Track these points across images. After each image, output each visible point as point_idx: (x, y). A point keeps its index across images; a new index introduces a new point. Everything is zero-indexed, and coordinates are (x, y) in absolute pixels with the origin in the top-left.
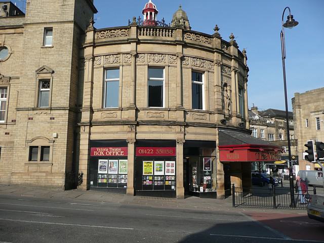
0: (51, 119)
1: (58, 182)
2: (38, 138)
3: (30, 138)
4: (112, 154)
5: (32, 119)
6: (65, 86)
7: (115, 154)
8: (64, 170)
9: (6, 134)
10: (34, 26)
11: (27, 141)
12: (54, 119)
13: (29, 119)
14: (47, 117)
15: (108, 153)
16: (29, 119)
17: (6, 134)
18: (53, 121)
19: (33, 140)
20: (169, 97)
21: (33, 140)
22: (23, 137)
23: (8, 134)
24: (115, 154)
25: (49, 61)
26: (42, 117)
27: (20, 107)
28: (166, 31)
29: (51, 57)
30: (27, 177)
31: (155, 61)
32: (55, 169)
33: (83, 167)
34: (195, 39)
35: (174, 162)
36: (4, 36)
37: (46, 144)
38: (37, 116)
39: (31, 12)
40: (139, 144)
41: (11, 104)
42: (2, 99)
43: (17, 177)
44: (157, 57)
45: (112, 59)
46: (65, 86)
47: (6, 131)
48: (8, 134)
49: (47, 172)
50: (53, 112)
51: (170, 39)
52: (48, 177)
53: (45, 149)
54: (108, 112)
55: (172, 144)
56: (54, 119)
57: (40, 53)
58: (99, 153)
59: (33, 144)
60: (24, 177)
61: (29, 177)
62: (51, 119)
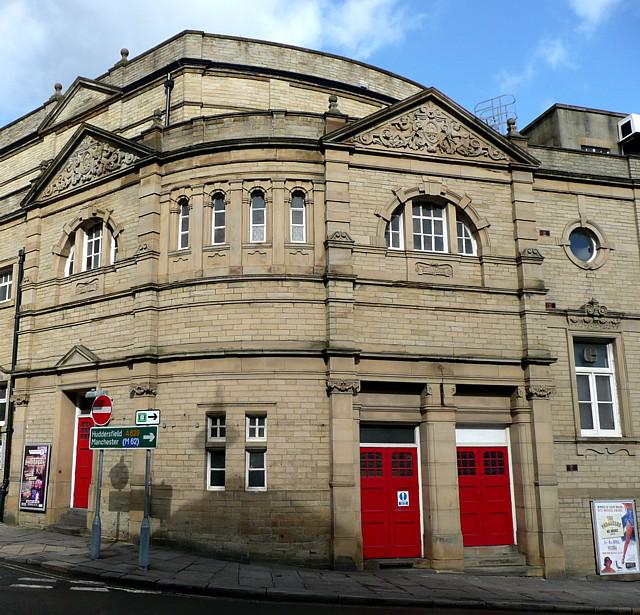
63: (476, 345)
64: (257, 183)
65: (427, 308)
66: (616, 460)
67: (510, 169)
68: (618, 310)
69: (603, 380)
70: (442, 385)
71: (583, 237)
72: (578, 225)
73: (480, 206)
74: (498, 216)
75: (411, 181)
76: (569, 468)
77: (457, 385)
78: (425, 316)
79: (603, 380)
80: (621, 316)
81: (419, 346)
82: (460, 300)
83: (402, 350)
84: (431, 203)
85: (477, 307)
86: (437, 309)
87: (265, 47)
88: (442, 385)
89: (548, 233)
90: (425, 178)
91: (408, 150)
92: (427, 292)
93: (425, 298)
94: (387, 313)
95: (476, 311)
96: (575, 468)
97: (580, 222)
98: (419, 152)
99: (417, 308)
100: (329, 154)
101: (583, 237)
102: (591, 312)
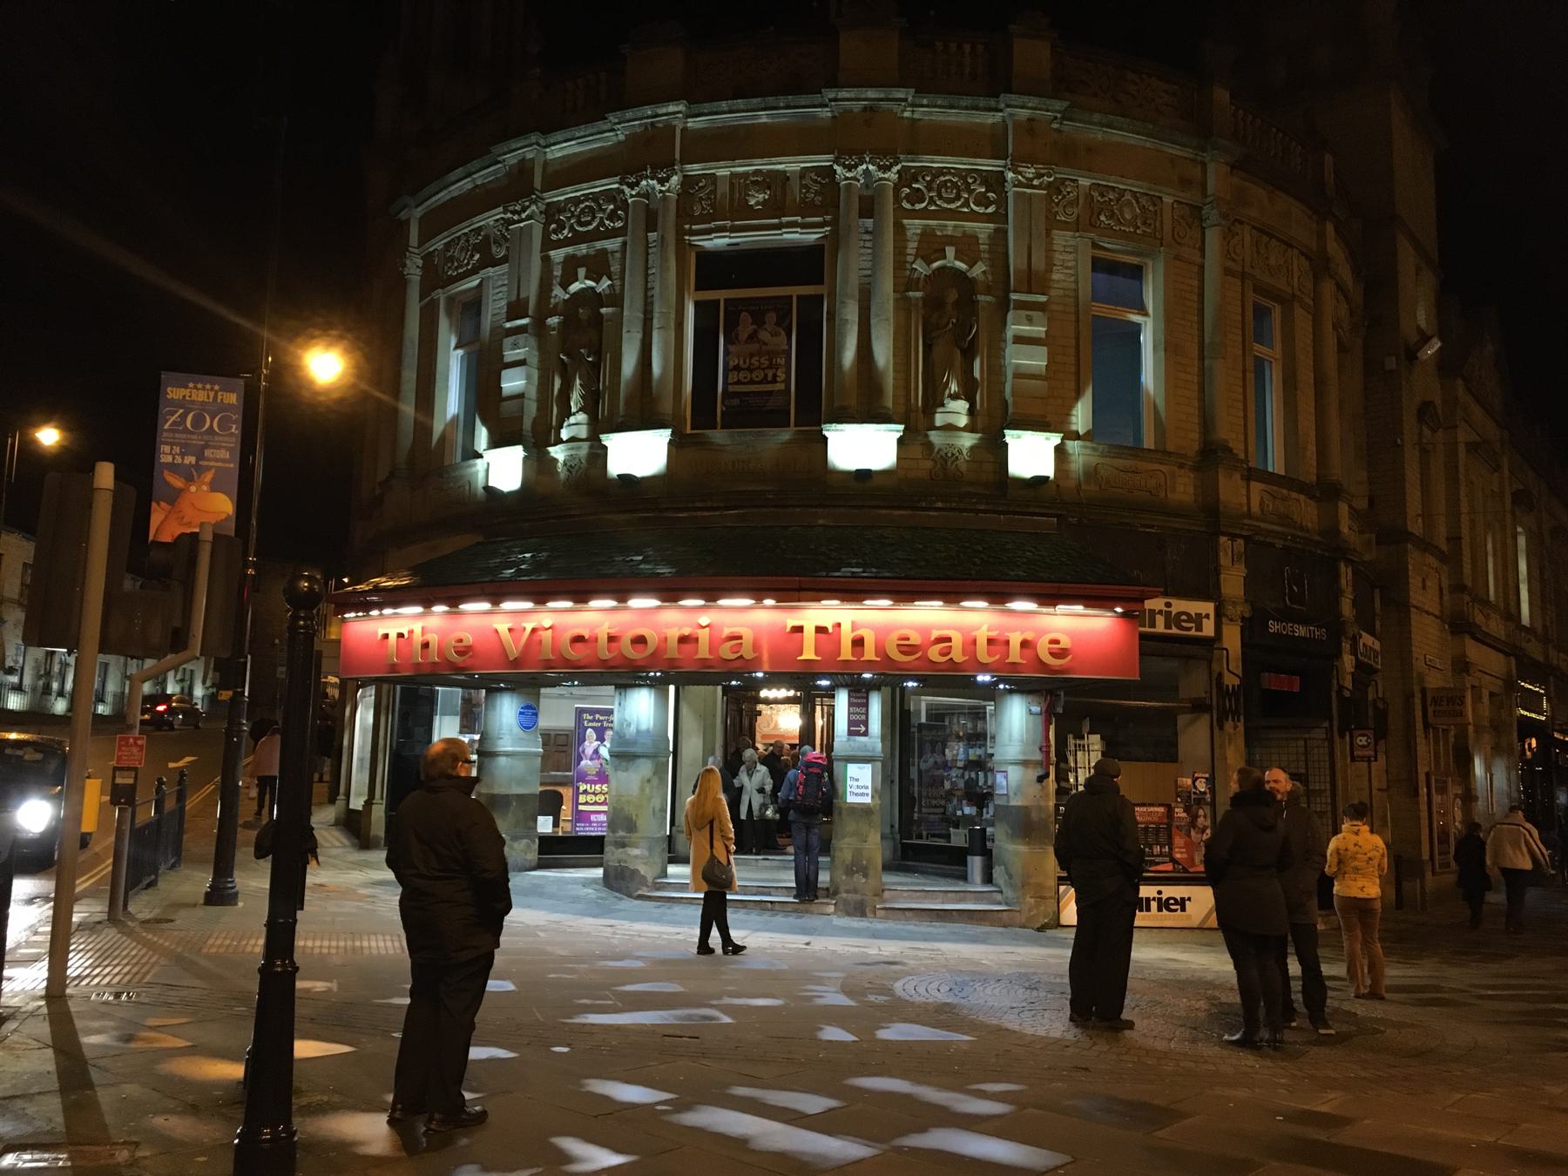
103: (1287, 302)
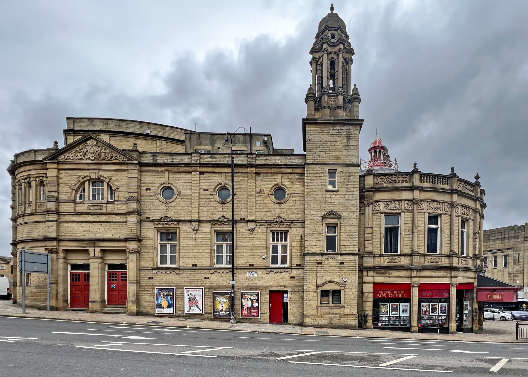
0: (341, 263)
1: (352, 323)
2: (330, 282)
3: (320, 282)
4: (395, 296)
5: (321, 263)
6: (353, 232)
7: (398, 296)
8: (356, 312)
9: (291, 277)
10: (317, 168)
11: (318, 286)
12: (343, 263)
13: (318, 263)
14: (337, 263)
15: (391, 296)
16: (318, 263)
17: (291, 277)
18: (342, 265)
19: (324, 284)
20: (404, 244)
21: (324, 284)
22: (313, 281)
23: (294, 277)
24: (398, 296)
25: (336, 204)
26: (331, 263)
27: (308, 252)
28: (427, 177)
29: (337, 202)
30: (320, 319)
31: (435, 209)
32: (347, 311)
33: (369, 308)
34: (390, 181)
35: (408, 304)
36: (280, 175)
37: (337, 287)
38: (326, 261)
39: (312, 150)
40: (423, 287)
41: (295, 248)
42: (273, 242)
43: (310, 319)
44: (435, 205)
45: (393, 205)
46: (353, 232)
47: (292, 275)
48: (294, 277)
49: (341, 314)
50: (343, 257)
51: (447, 187)
52: (341, 319)
53: (337, 294)
54: (391, 257)
55: (447, 287)
56: (343, 263)
57: (326, 197)
58: (382, 296)
59: (325, 288)
60: (316, 319)
61: (323, 319)
62: (341, 263)
63: (110, 235)
64: (41, 178)
65: (90, 222)
66: (171, 275)
67: (127, 164)
68: (179, 219)
69: (285, 247)
70: (94, 250)
71: (167, 189)
72: (221, 186)
73: (115, 181)
74: (123, 184)
75: (86, 173)
76: (149, 278)
77: (101, 250)
78: (88, 225)
79: (285, 247)
80: (180, 221)
81: (87, 236)
82: (104, 218)
83: (79, 237)
84: (99, 181)
85: (111, 220)
86: (93, 222)
87: (100, 120)
88: (94, 250)
89: (150, 189)
90: (91, 171)
91: (83, 161)
92: (90, 216)
93: (89, 218)
94: (73, 225)
95: (110, 222)
96: (152, 278)
97: (222, 184)
98: (88, 161)
99: (85, 222)
100: (49, 166)
101: (167, 189)
102: (166, 220)
103: (467, 220)
